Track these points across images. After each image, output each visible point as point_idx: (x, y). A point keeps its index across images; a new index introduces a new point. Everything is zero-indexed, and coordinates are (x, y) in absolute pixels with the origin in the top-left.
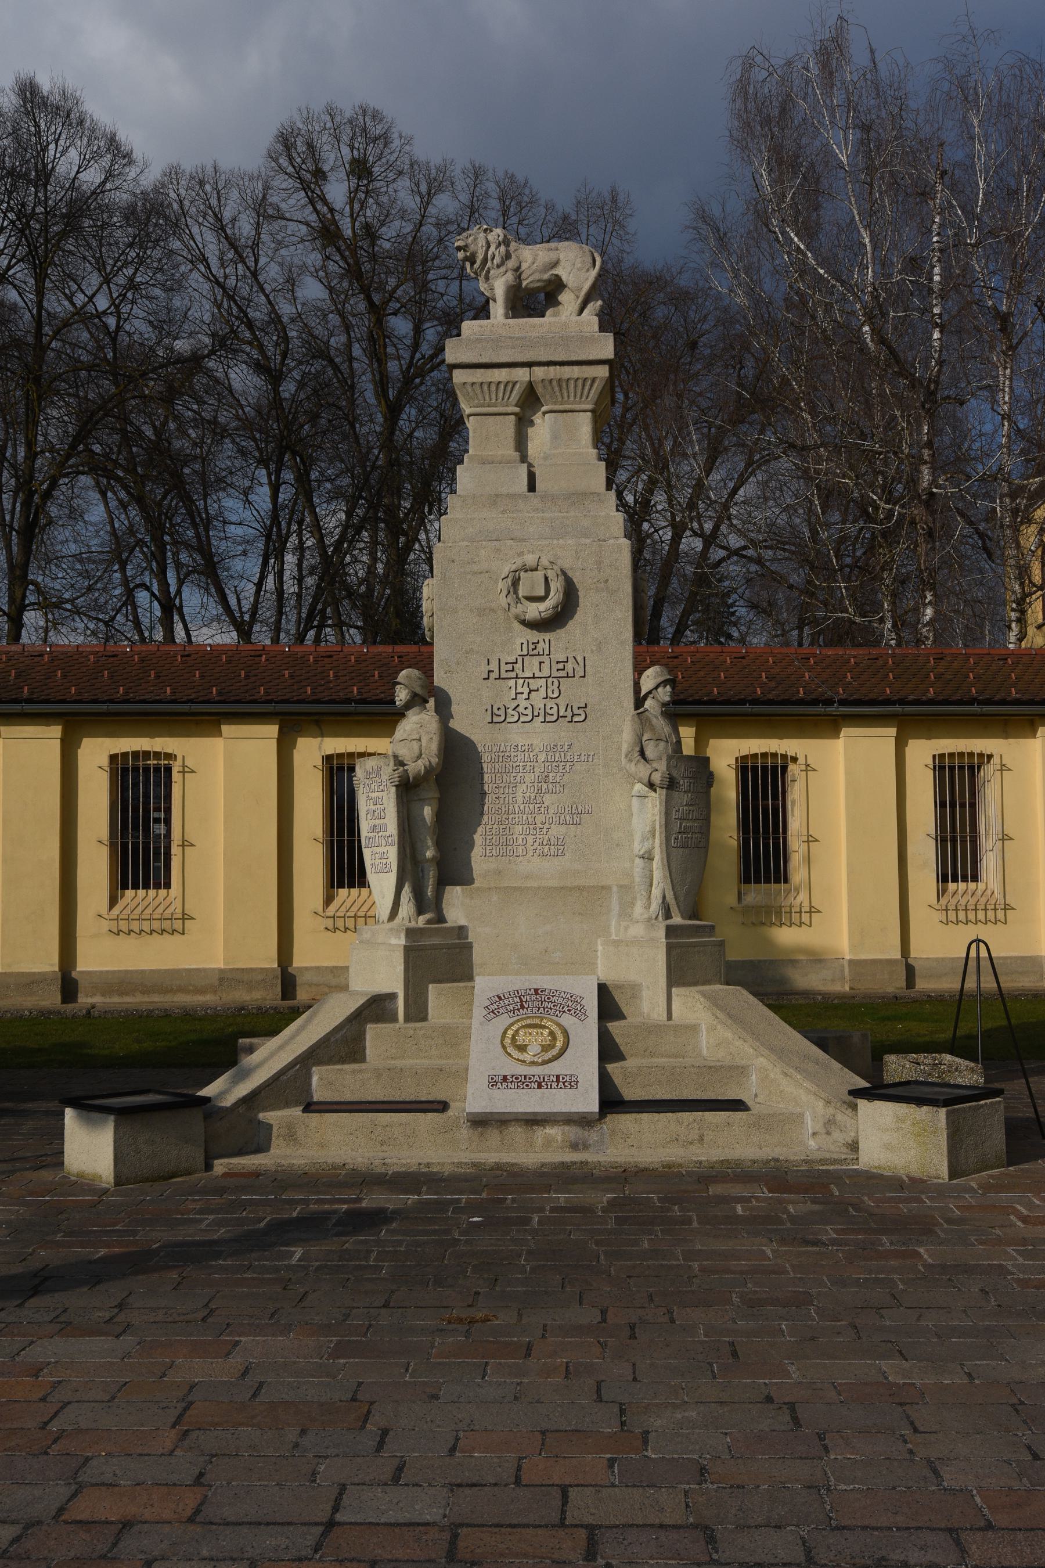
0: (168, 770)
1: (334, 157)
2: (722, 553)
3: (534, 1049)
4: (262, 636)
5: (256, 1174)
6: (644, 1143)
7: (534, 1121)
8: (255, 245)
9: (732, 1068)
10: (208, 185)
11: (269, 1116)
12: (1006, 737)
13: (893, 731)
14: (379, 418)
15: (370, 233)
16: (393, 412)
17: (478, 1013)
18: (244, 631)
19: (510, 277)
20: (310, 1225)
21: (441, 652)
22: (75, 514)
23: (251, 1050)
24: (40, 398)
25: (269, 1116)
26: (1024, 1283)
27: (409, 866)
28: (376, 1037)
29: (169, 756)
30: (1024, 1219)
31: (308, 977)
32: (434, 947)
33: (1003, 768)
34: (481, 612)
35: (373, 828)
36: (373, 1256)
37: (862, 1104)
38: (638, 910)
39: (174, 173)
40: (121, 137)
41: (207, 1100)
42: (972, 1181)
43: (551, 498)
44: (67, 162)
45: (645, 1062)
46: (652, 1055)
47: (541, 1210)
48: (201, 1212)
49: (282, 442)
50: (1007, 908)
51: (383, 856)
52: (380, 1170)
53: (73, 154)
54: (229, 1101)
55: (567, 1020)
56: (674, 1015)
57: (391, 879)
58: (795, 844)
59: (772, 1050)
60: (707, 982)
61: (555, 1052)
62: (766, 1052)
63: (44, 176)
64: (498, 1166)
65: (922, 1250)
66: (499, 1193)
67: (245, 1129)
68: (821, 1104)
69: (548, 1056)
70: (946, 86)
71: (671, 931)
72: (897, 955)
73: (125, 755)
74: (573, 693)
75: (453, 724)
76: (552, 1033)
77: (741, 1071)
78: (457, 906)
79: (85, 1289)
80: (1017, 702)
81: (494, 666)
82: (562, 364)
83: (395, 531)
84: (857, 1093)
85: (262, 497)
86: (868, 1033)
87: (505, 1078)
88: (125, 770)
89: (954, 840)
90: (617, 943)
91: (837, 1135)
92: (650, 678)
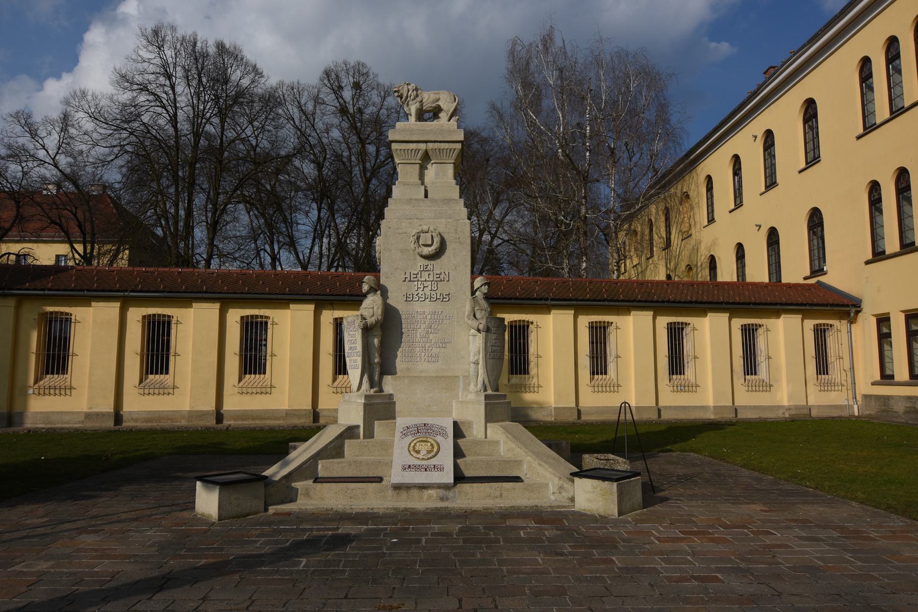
0: (266, 323)
1: (347, 81)
2: (500, 241)
3: (423, 452)
4: (311, 269)
5: (289, 514)
6: (474, 498)
7: (423, 487)
8: (314, 114)
9: (515, 461)
10: (296, 90)
11: (298, 485)
12: (618, 315)
13: (573, 312)
14: (362, 186)
15: (360, 111)
16: (368, 181)
17: (398, 435)
18: (305, 267)
19: (418, 105)
20: (312, 545)
21: (384, 268)
22: (236, 219)
23: (295, 448)
24: (221, 170)
25: (298, 485)
26: (669, 579)
27: (367, 365)
28: (349, 446)
29: (266, 317)
30: (658, 539)
31: (325, 413)
32: (378, 404)
33: (617, 328)
34: (402, 251)
35: (351, 348)
36: (342, 564)
37: (576, 479)
38: (472, 387)
39: (281, 84)
40: (258, 66)
41: (266, 477)
42: (629, 517)
43: (434, 201)
44: (235, 75)
45: (476, 458)
46: (478, 455)
47: (427, 534)
48: (259, 536)
49: (323, 192)
50: (618, 386)
51: (355, 361)
52: (349, 511)
53: (238, 73)
54: (277, 478)
55: (439, 438)
56: (488, 436)
57: (359, 372)
58: (532, 358)
59: (533, 453)
60: (503, 421)
61: (433, 454)
62: (531, 454)
63: (226, 81)
64: (406, 509)
65: (614, 558)
66: (405, 524)
67: (284, 491)
68: (557, 479)
69: (430, 455)
70: (590, 59)
71: (487, 397)
72: (574, 405)
73: (247, 316)
74: (443, 288)
75: (388, 301)
76: (432, 445)
77: (519, 463)
78: (389, 385)
79: (188, 587)
80: (623, 301)
81: (408, 275)
82: (441, 142)
83: (368, 229)
84: (574, 474)
85: (314, 214)
86: (575, 442)
87: (409, 466)
88: (247, 323)
89: (597, 358)
90: (462, 402)
91: (564, 494)
92: (478, 282)
